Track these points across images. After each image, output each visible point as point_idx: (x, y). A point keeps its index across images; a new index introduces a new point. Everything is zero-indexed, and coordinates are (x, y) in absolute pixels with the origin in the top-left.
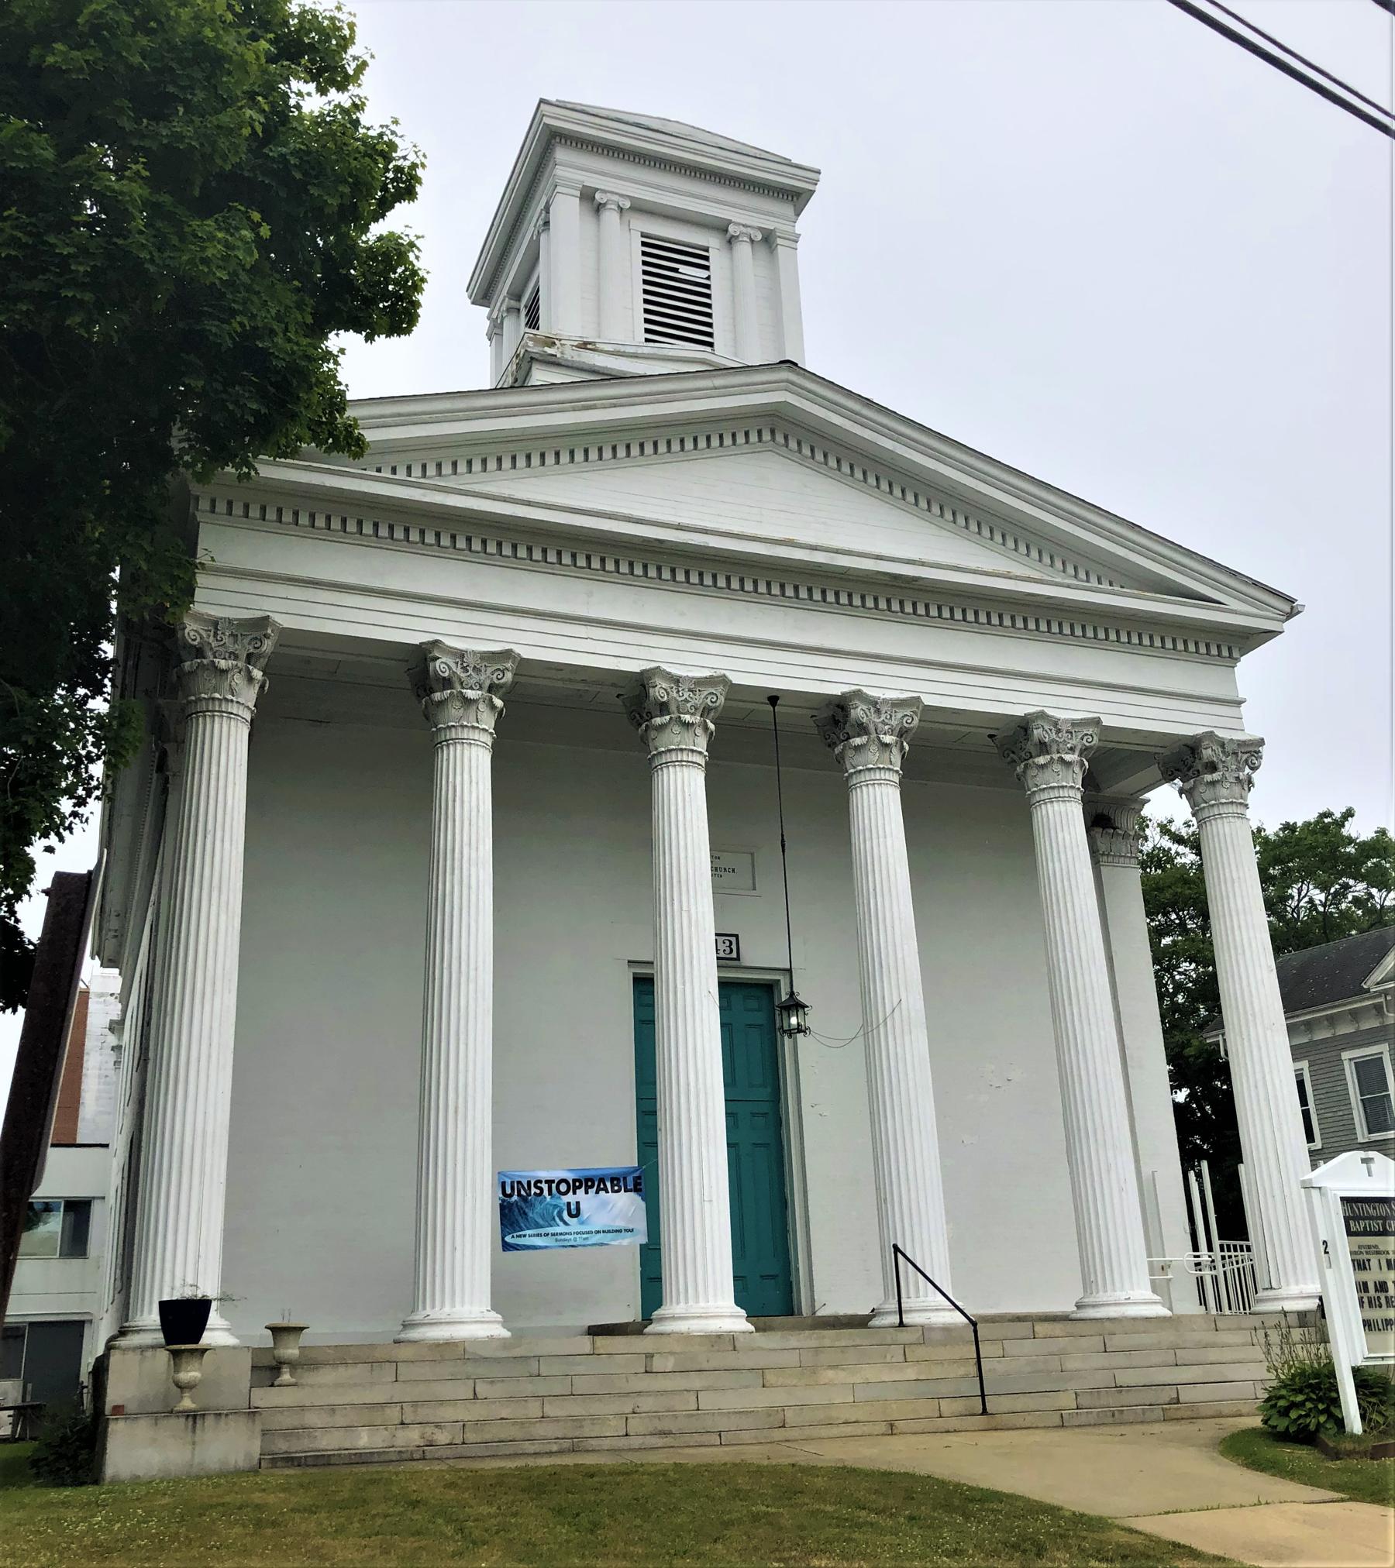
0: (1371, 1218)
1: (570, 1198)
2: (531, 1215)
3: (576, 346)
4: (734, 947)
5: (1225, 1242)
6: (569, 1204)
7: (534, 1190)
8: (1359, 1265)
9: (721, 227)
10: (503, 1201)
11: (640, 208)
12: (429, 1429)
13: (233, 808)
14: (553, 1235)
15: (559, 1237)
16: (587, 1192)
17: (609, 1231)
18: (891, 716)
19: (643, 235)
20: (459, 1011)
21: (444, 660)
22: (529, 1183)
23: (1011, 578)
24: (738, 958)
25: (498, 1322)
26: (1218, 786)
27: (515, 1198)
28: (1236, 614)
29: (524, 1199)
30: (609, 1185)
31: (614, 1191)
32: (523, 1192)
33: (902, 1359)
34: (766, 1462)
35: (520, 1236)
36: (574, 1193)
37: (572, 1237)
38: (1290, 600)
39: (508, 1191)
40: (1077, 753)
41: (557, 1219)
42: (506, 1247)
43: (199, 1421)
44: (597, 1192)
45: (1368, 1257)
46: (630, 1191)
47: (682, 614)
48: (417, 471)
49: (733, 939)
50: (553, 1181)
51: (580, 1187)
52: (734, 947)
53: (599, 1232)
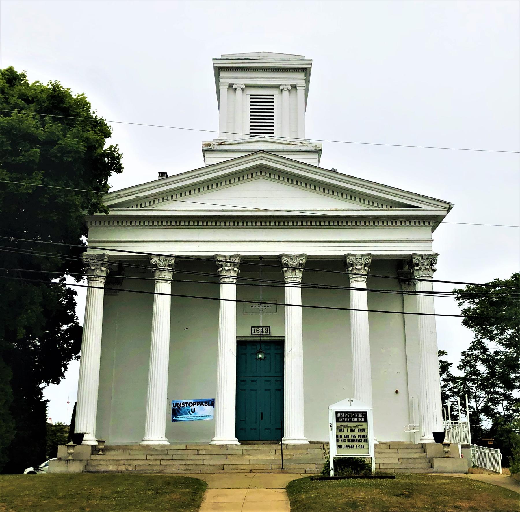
0: (347, 417)
1: (192, 407)
2: (181, 412)
3: (218, 144)
4: (269, 330)
5: (454, 422)
6: (192, 409)
7: (182, 405)
8: (340, 430)
9: (277, 87)
10: (173, 408)
11: (248, 86)
12: (127, 466)
13: (97, 307)
14: (187, 417)
15: (188, 418)
16: (197, 406)
17: (203, 416)
18: (296, 260)
19: (251, 95)
20: (156, 358)
21: (154, 259)
22: (181, 403)
23: (337, 211)
24: (270, 334)
25: (237, 441)
26: (419, 271)
27: (176, 407)
28: (428, 210)
29: (179, 408)
30: (204, 404)
31: (205, 405)
32: (179, 406)
33: (274, 453)
34: (193, 477)
35: (177, 418)
36: (194, 406)
37: (192, 418)
38: (450, 204)
39: (175, 406)
40: (363, 265)
41: (188, 413)
42: (173, 420)
43: (68, 461)
44: (200, 406)
45: (343, 428)
46: (210, 405)
47: (228, 236)
48: (139, 206)
49: (269, 328)
50: (188, 403)
51: (195, 404)
52: (269, 330)
53: (200, 416)
